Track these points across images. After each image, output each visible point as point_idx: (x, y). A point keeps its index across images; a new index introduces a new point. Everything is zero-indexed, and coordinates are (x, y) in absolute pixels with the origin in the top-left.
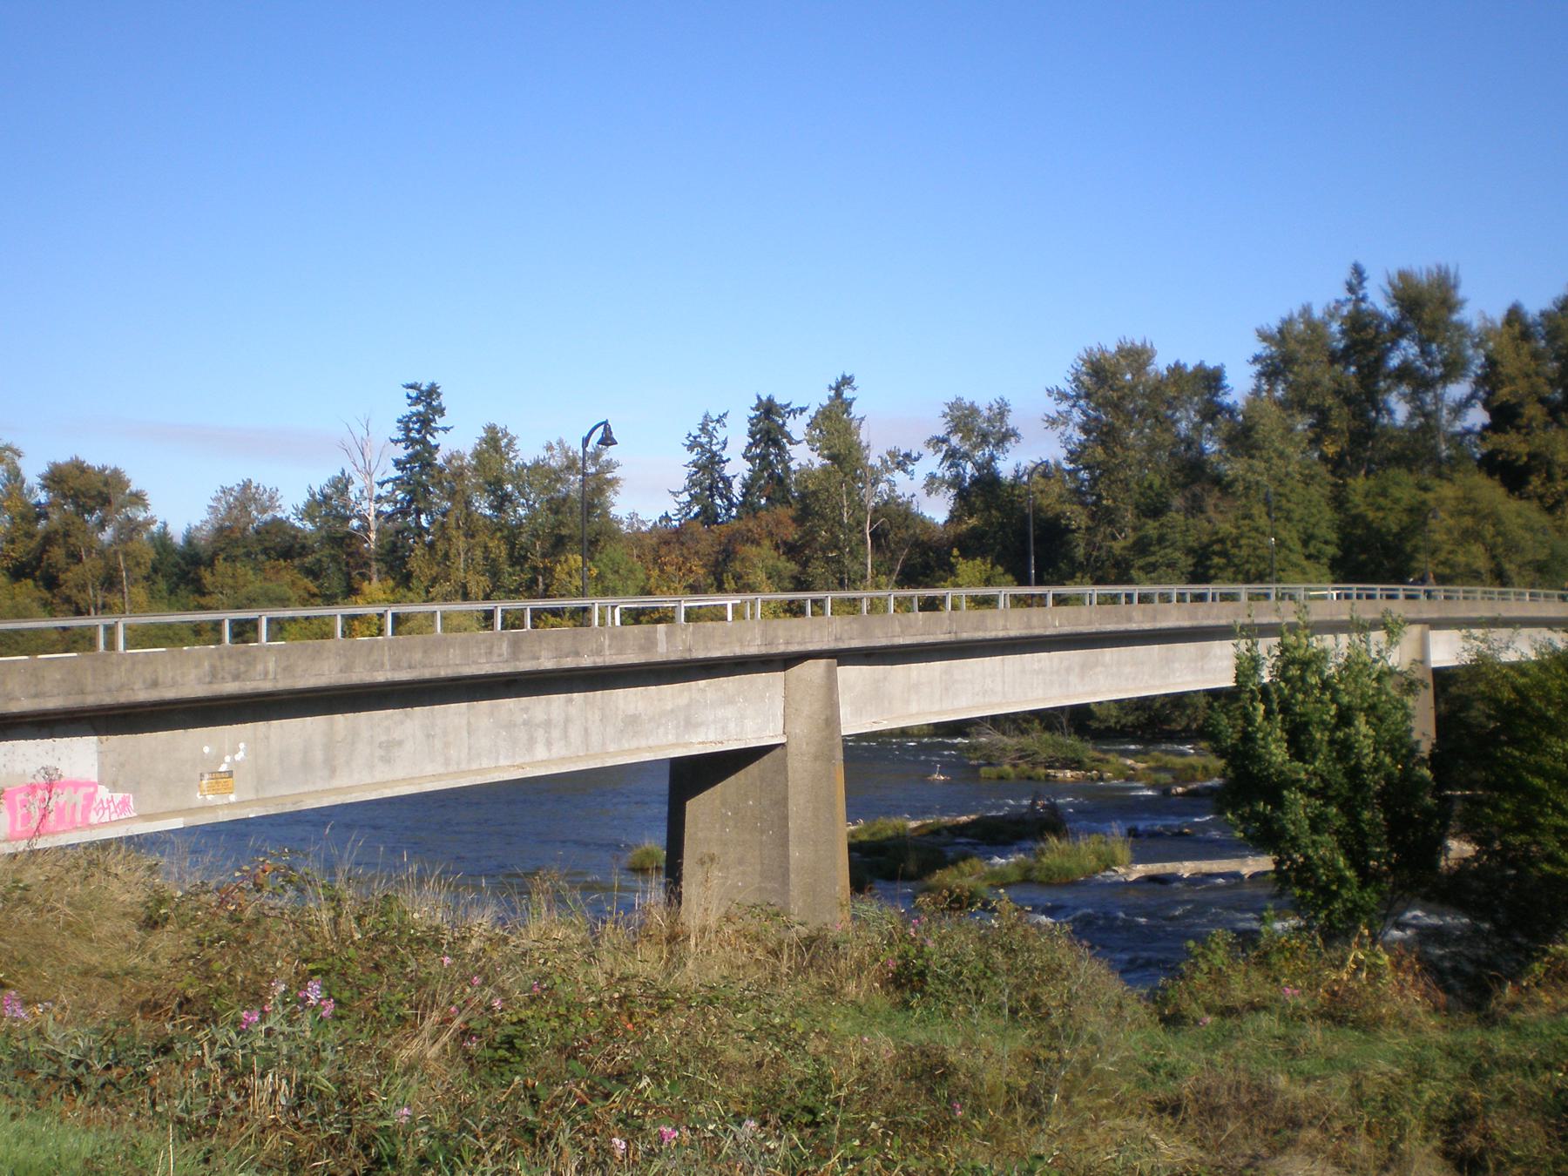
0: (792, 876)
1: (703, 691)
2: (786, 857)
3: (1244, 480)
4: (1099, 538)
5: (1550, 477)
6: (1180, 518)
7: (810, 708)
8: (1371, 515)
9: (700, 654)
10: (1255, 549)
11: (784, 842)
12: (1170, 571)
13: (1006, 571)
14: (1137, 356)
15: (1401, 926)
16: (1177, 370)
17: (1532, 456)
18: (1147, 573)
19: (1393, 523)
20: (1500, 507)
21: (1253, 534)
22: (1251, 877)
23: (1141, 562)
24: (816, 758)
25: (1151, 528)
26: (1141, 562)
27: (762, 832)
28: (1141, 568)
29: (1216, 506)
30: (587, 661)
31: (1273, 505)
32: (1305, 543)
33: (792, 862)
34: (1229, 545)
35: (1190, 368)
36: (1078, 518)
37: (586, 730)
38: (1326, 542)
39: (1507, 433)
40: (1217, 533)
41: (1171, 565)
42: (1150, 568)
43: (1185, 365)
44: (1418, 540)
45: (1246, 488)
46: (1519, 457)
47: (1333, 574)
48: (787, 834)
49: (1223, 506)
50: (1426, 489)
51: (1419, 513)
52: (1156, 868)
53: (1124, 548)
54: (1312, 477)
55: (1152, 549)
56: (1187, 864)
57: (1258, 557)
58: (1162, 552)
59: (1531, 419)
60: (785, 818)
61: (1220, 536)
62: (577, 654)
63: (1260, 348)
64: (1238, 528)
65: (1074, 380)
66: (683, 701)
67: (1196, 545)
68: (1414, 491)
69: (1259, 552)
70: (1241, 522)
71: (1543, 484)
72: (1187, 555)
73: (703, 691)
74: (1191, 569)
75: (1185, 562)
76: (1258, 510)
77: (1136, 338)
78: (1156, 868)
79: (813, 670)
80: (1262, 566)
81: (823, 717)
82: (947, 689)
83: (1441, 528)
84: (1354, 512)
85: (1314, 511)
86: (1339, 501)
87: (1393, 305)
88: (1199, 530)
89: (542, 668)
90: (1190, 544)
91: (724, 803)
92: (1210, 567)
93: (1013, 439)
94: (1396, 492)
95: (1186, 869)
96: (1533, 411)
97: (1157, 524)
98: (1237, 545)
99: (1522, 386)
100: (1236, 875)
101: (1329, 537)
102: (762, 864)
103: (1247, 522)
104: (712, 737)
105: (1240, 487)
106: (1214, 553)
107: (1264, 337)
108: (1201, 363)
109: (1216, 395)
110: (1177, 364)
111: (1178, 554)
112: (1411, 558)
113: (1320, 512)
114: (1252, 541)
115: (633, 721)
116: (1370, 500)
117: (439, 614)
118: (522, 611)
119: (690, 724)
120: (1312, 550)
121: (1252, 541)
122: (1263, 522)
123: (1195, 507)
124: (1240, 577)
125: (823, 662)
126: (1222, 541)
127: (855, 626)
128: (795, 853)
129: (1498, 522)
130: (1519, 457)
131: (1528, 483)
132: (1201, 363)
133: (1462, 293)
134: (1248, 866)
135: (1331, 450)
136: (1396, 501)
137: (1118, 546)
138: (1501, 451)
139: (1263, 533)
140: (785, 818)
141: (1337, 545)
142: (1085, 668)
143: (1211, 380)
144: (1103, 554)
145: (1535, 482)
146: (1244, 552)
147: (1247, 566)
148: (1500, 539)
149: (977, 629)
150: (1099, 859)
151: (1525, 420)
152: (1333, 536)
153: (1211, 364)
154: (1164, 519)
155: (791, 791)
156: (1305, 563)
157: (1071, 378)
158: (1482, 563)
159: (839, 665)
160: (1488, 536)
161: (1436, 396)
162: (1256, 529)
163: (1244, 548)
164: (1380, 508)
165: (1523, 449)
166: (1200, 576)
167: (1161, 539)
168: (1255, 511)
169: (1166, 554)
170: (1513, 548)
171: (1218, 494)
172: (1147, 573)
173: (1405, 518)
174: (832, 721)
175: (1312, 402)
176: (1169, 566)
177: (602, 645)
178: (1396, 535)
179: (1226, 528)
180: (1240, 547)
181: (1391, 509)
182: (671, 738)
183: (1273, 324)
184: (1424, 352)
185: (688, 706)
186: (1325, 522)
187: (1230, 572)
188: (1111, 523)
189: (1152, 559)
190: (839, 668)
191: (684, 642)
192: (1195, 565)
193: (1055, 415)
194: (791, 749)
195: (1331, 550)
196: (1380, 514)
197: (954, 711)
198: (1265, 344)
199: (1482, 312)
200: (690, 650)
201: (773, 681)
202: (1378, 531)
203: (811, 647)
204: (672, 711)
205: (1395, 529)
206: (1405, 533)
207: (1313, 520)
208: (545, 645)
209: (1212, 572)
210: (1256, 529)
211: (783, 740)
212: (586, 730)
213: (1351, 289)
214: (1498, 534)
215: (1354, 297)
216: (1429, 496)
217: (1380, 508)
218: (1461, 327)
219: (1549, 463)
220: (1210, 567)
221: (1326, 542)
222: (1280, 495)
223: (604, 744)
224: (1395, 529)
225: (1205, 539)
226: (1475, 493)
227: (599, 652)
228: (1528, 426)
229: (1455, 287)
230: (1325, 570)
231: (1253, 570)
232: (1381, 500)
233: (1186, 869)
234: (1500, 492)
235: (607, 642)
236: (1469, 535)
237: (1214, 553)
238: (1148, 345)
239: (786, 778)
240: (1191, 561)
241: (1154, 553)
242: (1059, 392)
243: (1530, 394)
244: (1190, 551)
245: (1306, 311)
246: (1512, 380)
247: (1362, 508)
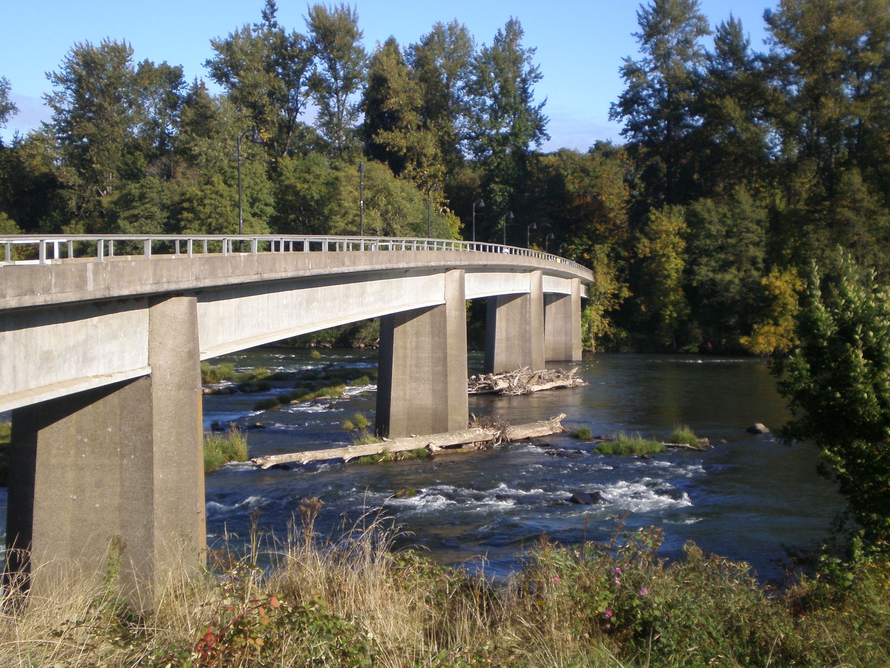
0: (156, 496)
1: (96, 326)
2: (151, 480)
3: (206, 154)
4: (88, 194)
5: (420, 165)
6: (156, 181)
7: (174, 341)
8: (299, 186)
9: (116, 292)
10: (216, 207)
11: (148, 465)
12: (149, 221)
13: (11, 217)
14: (120, 53)
15: (877, 546)
16: (146, 67)
17: (409, 149)
18: (131, 223)
19: (316, 192)
20: (390, 184)
21: (214, 196)
22: (349, 461)
23: (127, 214)
24: (179, 387)
25: (133, 188)
26: (127, 214)
27: (123, 456)
28: (125, 218)
29: (184, 174)
30: (40, 299)
31: (228, 174)
32: (252, 205)
33: (156, 482)
34: (195, 203)
35: (156, 66)
36: (70, 176)
37: (14, 367)
38: (266, 205)
39: (392, 131)
40: (183, 194)
41: (150, 217)
42: (134, 218)
43: (153, 63)
44: (333, 206)
45: (207, 160)
46: (400, 149)
47: (270, 227)
48: (151, 458)
49: (189, 173)
50: (336, 169)
51: (333, 185)
52: (284, 458)
53: (112, 202)
54: (254, 156)
55: (134, 204)
56: (307, 453)
57: (218, 213)
58: (143, 207)
59: (409, 122)
60: (149, 444)
61: (188, 196)
62: (32, 292)
63: (213, 55)
64: (202, 191)
65: (67, 67)
66: (81, 337)
67: (169, 202)
68: (329, 171)
69: (219, 210)
70: (204, 187)
71: (414, 169)
72: (162, 210)
73: (96, 326)
74: (165, 220)
75: (161, 215)
76: (217, 179)
77: (117, 38)
78: (284, 458)
79: (177, 307)
80: (221, 220)
81: (187, 350)
82: (238, 322)
83: (349, 195)
84: (286, 183)
85: (259, 181)
86: (274, 172)
87: (312, 31)
88: (170, 191)
89: (8, 307)
90: (165, 201)
91: (80, 431)
92: (182, 220)
93: (11, 112)
94: (316, 170)
95: (306, 457)
96: (411, 117)
97: (138, 185)
98: (201, 202)
99: (402, 99)
100: (341, 460)
101: (268, 201)
102: (122, 486)
103: (208, 187)
104: (102, 371)
105: (203, 159)
106: (185, 209)
107: (216, 46)
108: (165, 63)
109: (176, 88)
110: (146, 61)
111: (155, 209)
112: (327, 218)
113: (262, 182)
114: (213, 202)
115: (47, 357)
116: (297, 175)
117: (8, 248)
118: (173, 242)
119: (87, 360)
120: (256, 210)
121: (213, 202)
122: (222, 187)
123: (168, 174)
124: (204, 228)
125: (185, 300)
126: (190, 200)
127: (207, 267)
128: (159, 475)
129: (389, 194)
130: (400, 149)
131: (405, 168)
132: (165, 63)
133: (361, 26)
134: (349, 453)
135: (266, 136)
136: (318, 177)
137: (106, 201)
138: (388, 144)
139: (222, 196)
140: (150, 443)
141: (274, 207)
142: (309, 302)
143: (174, 76)
144: (91, 206)
145: (410, 167)
146: (208, 210)
147: (210, 220)
148: (390, 207)
149: (271, 271)
150: (224, 452)
151: (405, 123)
152: (271, 200)
153: (172, 64)
154: (142, 181)
155: (156, 418)
156: (252, 219)
157: (63, 66)
158: (379, 224)
159: (199, 301)
160: (382, 205)
161: (338, 101)
162: (217, 193)
163: (207, 206)
164: (306, 181)
165: (403, 143)
166: (173, 227)
167: (142, 197)
168: (215, 179)
169: (146, 208)
170: (399, 211)
171: (185, 165)
172: (131, 223)
173: (324, 189)
174: (193, 353)
175: (251, 99)
176: (147, 218)
177: (50, 283)
178: (317, 202)
179: (194, 190)
180: (204, 206)
181: (313, 183)
182: (73, 374)
183: (223, 36)
184: (332, 68)
185: (86, 341)
186: (266, 191)
187: (196, 224)
188: (97, 182)
189: (136, 212)
190: (198, 304)
191: (104, 279)
192: (168, 218)
193: (53, 95)
194: (156, 379)
195: (270, 211)
196: (306, 186)
197: (237, 343)
198: (217, 52)
199: (513, 29)
200: (108, 288)
201: (140, 316)
202: (304, 197)
203: (173, 287)
204: (74, 346)
205: (316, 197)
206: (322, 202)
207: (257, 188)
208: (10, 283)
209: (183, 224)
210: (217, 193)
211: (147, 371)
212: (14, 367)
213: (265, 16)
214: (389, 203)
215: (267, 23)
216: (341, 174)
217: (306, 181)
218: (360, 52)
219: (420, 155)
220: (182, 220)
221: (266, 205)
222: (233, 168)
223: (27, 381)
224: (316, 197)
225: (177, 198)
226: (373, 173)
227: (47, 290)
228: (406, 127)
229: (354, 21)
230: (265, 225)
231: (214, 224)
232: (307, 176)
233: (306, 457)
234: (389, 174)
235: (53, 280)
236: (371, 203)
237: (185, 209)
238: (128, 46)
239: (151, 407)
240: (166, 214)
241: (134, 208)
242: (56, 76)
243: (407, 105)
244: (163, 207)
245: (246, 30)
246: (397, 93)
247: (292, 181)
